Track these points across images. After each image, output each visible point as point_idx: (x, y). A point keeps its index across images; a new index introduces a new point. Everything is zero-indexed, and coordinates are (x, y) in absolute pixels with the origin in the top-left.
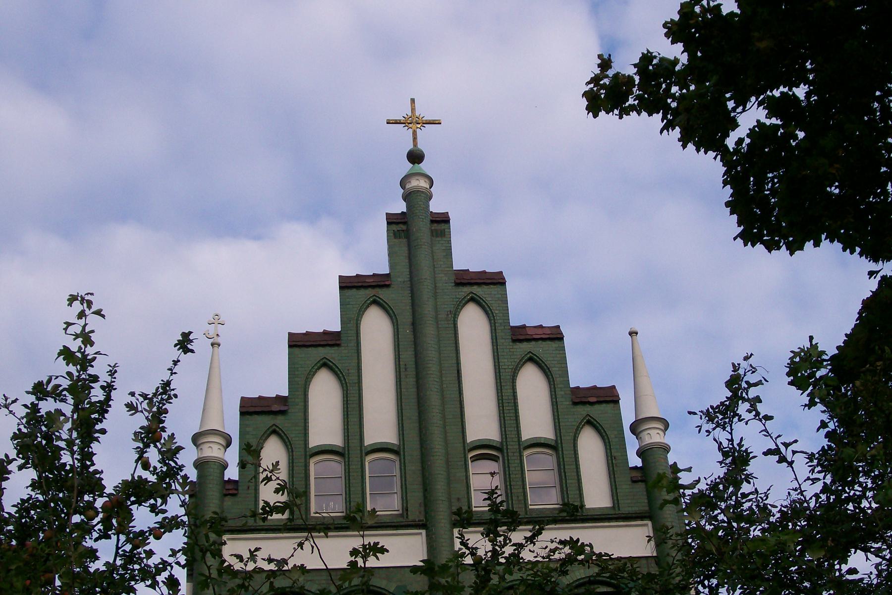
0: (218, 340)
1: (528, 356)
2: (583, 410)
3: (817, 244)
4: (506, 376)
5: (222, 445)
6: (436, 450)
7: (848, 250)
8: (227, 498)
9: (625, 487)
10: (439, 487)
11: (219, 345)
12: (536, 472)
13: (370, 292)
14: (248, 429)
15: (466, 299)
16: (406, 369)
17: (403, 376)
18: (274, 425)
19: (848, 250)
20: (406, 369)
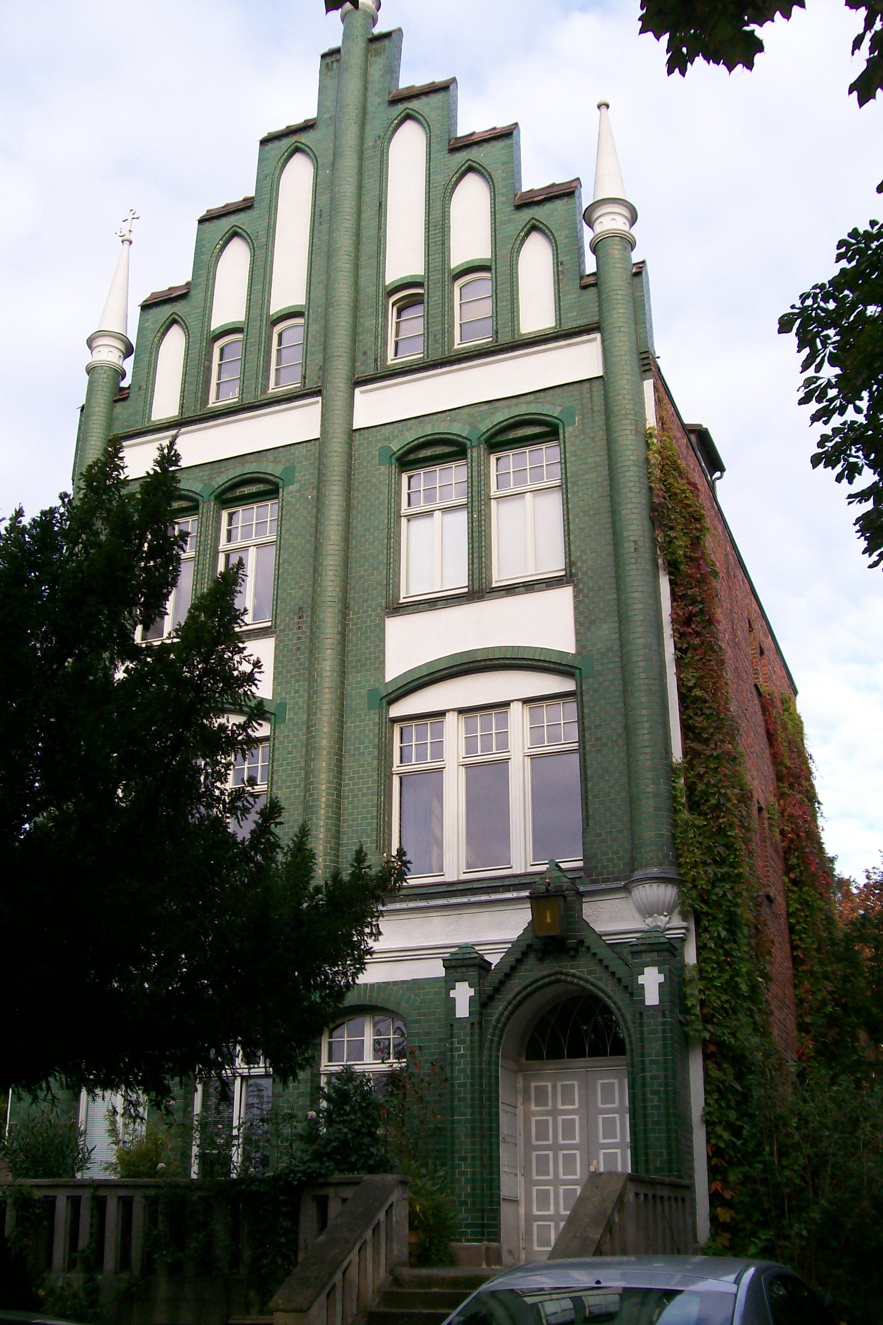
0: (132, 237)
1: (467, 165)
2: (527, 215)
3: (63, 496)
4: (437, 193)
5: (625, 216)
6: (345, 333)
7: (677, 70)
8: (118, 405)
9: (572, 294)
10: (330, 528)
11: (131, 243)
12: (482, 302)
13: (286, 143)
14: (146, 325)
15: (391, 129)
16: (321, 216)
17: (317, 224)
18: (174, 313)
19: (677, 70)
20: (321, 216)
